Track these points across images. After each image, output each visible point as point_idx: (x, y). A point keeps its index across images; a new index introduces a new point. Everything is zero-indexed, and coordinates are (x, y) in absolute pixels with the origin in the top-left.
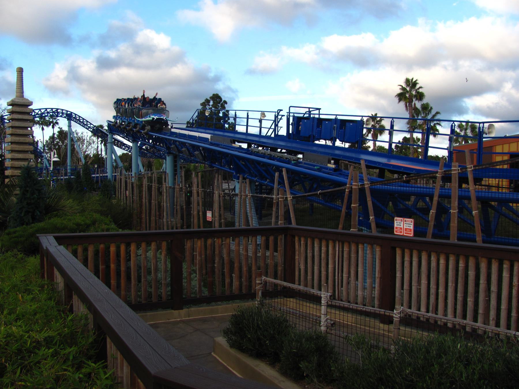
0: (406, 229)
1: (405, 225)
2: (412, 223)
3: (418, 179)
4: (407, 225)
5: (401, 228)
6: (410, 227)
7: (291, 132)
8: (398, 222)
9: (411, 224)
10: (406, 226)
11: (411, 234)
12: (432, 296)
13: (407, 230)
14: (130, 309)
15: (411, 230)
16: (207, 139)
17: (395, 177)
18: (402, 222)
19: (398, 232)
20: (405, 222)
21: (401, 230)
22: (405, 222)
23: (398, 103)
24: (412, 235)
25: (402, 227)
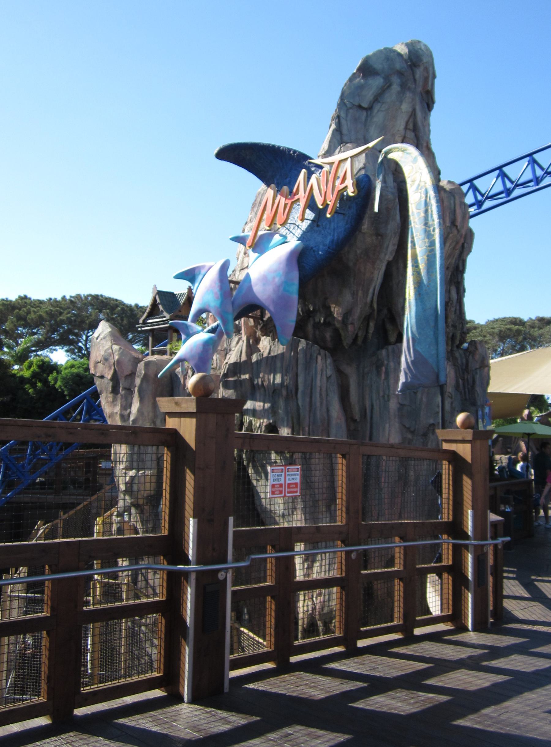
0: (289, 485)
1: (288, 477)
2: (299, 473)
3: (125, 514)
4: (291, 477)
5: (281, 485)
6: (296, 479)
7: (515, 576)
8: (277, 474)
9: (297, 475)
10: (289, 479)
11: (296, 492)
12: (184, 405)
13: (292, 486)
14: (254, 740)
15: (296, 484)
16: (92, 583)
17: (98, 526)
18: (283, 474)
19: (276, 493)
20: (287, 473)
21: (280, 489)
22: (287, 473)
23: (155, 285)
24: (298, 494)
25: (282, 482)
